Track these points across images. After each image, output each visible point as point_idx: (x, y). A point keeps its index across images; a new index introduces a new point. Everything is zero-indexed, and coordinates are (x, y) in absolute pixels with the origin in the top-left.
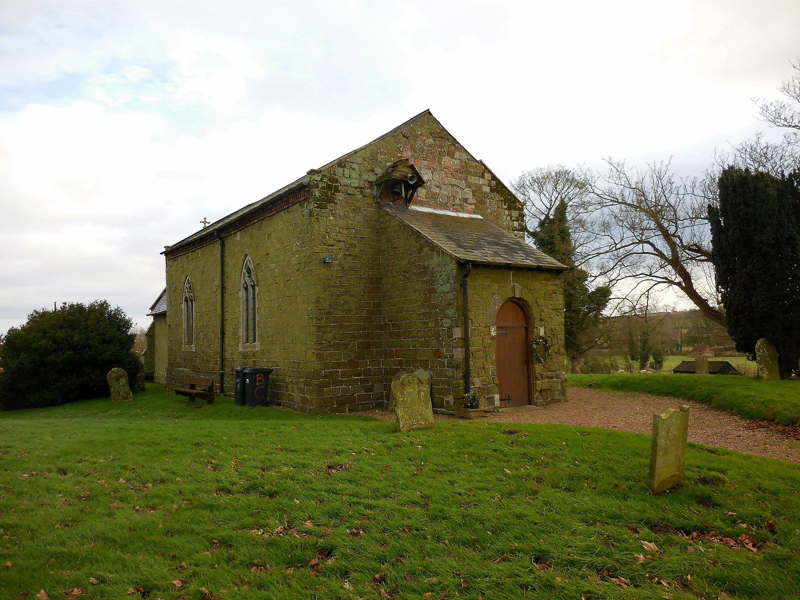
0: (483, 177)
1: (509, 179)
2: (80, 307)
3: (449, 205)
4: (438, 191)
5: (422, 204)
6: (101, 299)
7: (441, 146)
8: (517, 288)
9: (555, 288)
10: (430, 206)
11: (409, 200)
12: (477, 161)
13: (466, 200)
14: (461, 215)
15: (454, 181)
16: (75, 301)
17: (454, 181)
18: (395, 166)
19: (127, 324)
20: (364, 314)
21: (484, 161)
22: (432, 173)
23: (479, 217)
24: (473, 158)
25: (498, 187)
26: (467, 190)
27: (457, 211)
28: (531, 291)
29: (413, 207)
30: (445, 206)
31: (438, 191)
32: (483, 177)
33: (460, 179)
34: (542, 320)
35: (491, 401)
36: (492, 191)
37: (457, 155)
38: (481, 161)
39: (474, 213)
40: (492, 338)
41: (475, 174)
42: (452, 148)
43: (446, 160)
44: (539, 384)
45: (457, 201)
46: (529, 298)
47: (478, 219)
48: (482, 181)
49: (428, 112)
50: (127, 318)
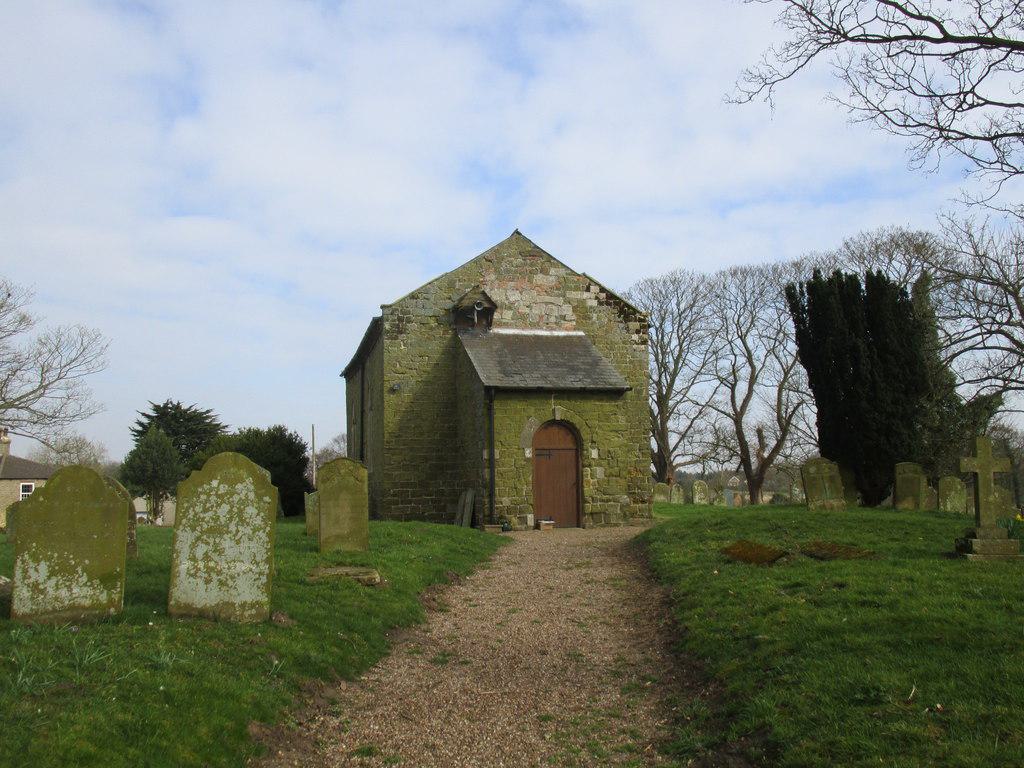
0: (588, 290)
1: (619, 290)
2: (257, 433)
3: (541, 323)
4: (527, 310)
5: (506, 325)
6: (278, 422)
7: (531, 265)
8: (560, 410)
9: (615, 409)
10: (517, 327)
11: (490, 324)
12: (579, 275)
13: (564, 318)
14: (556, 333)
15: (548, 299)
16: (254, 426)
17: (548, 299)
18: (462, 299)
19: (302, 448)
20: (437, 437)
21: (589, 274)
22: (521, 293)
23: (581, 333)
24: (573, 273)
25: (611, 299)
26: (565, 307)
27: (552, 329)
28: (580, 414)
29: (496, 330)
30: (534, 326)
31: (527, 310)
32: (588, 290)
33: (559, 296)
34: (593, 442)
35: (523, 520)
36: (600, 303)
37: (552, 271)
38: (584, 274)
39: (575, 330)
40: (527, 460)
41: (577, 289)
42: (547, 264)
43: (539, 278)
44: (589, 507)
45: (553, 319)
46: (576, 420)
47: (580, 337)
48: (586, 295)
49: (517, 232)
50: (303, 442)
